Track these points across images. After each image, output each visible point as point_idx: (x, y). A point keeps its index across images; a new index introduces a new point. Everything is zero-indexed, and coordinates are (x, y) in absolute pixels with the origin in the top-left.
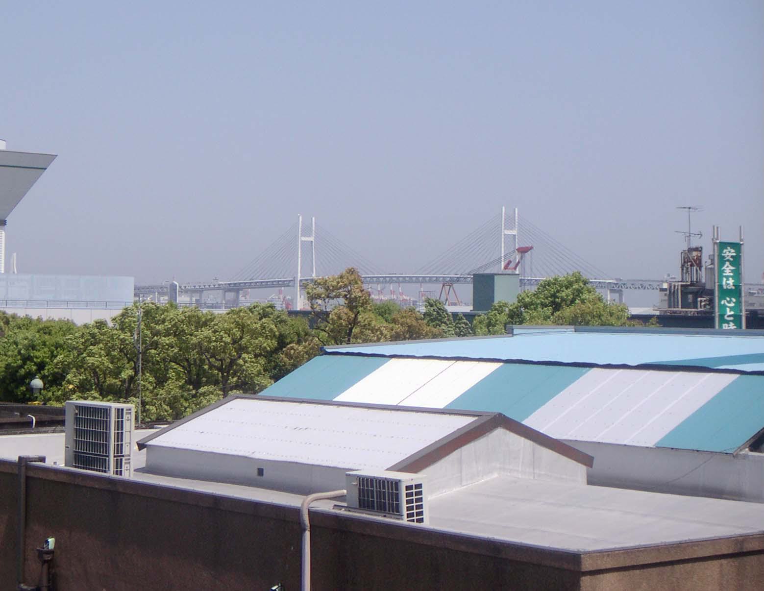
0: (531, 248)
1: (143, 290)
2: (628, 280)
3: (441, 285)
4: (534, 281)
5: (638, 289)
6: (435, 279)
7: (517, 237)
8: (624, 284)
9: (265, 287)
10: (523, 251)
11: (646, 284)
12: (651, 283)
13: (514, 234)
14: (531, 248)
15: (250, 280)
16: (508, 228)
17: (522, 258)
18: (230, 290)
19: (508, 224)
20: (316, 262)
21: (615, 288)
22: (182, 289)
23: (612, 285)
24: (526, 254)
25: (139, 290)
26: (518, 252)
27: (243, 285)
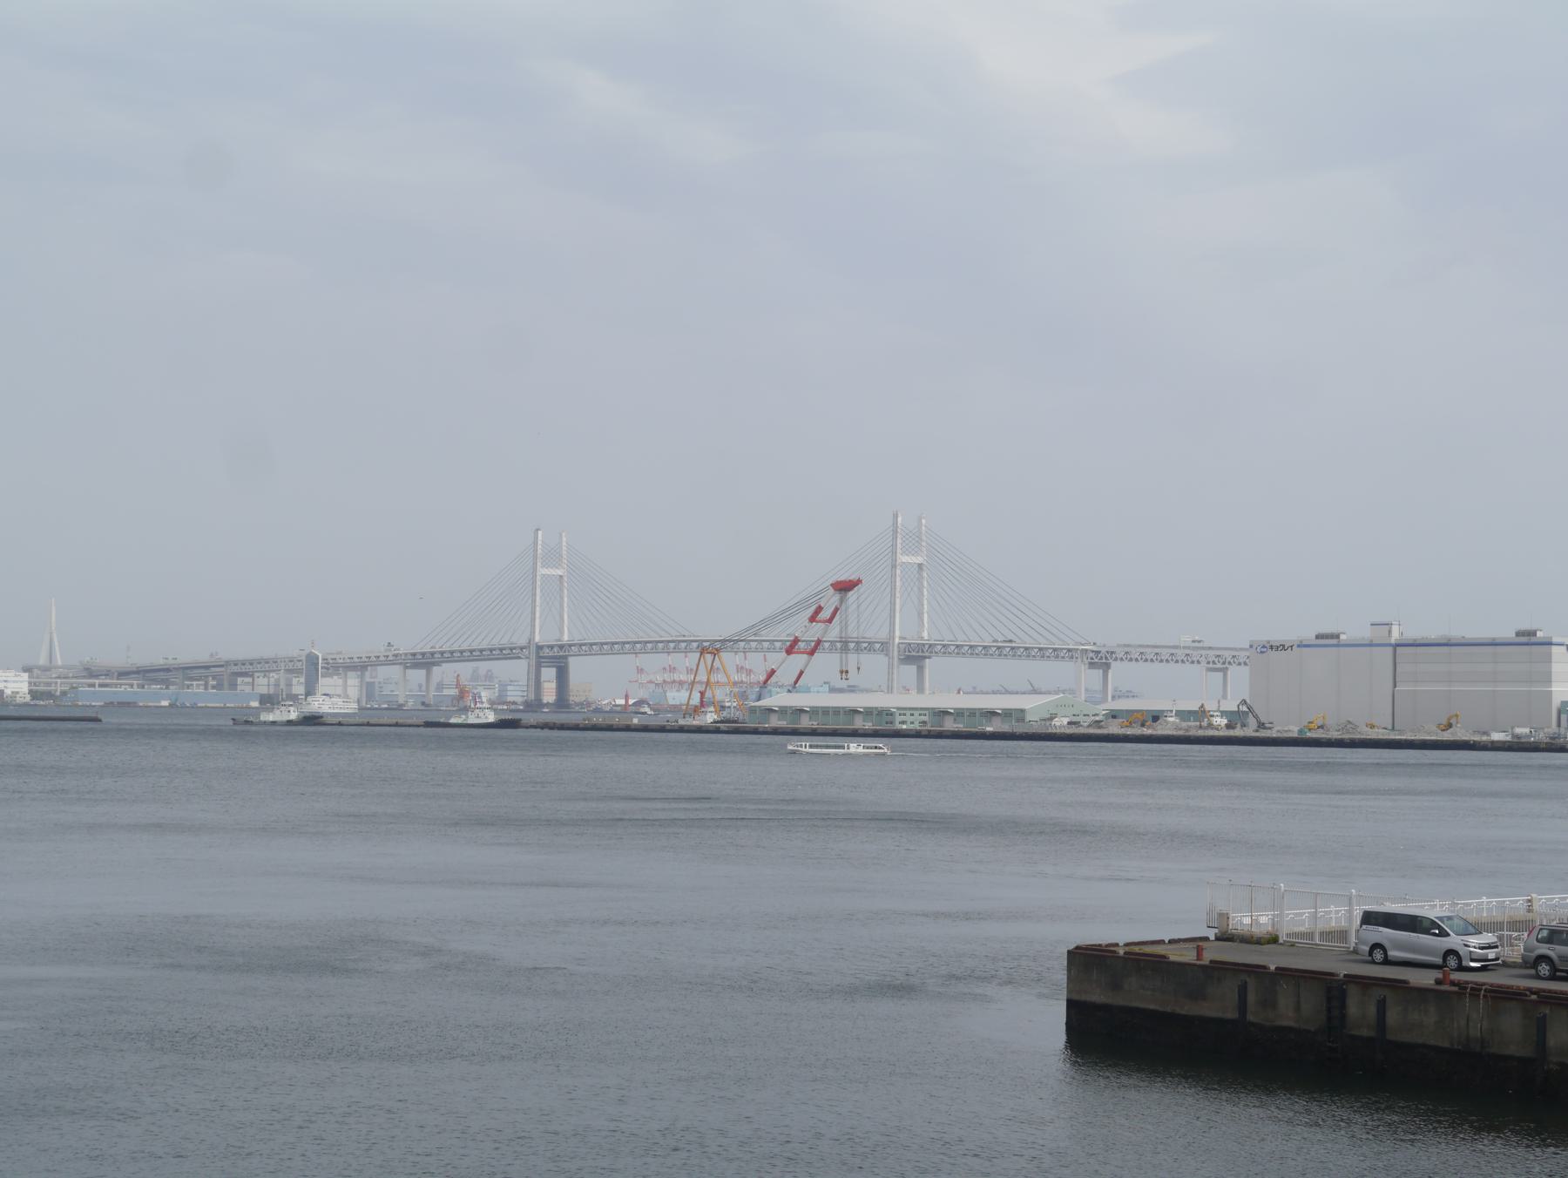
0: (859, 582)
1: (267, 665)
2: (1119, 646)
3: (698, 654)
4: (980, 648)
5: (1149, 663)
6: (865, 645)
7: (565, 579)
8: (1112, 653)
9: (468, 661)
10: (844, 587)
11: (1150, 653)
12: (1174, 651)
13: (561, 574)
14: (859, 582)
15: (432, 648)
16: (913, 552)
17: (842, 601)
18: (416, 666)
19: (907, 544)
20: (569, 617)
21: (1096, 660)
22: (328, 663)
23: (1091, 655)
24: (851, 593)
25: (251, 664)
26: (835, 590)
27: (478, 653)
